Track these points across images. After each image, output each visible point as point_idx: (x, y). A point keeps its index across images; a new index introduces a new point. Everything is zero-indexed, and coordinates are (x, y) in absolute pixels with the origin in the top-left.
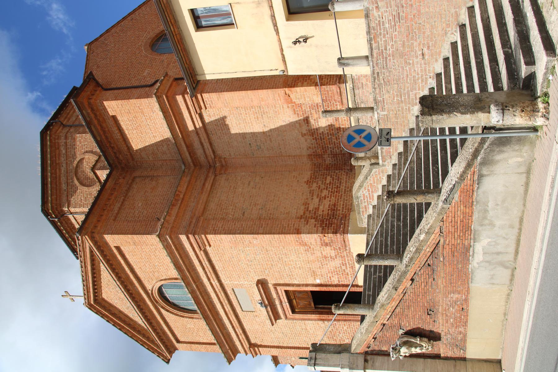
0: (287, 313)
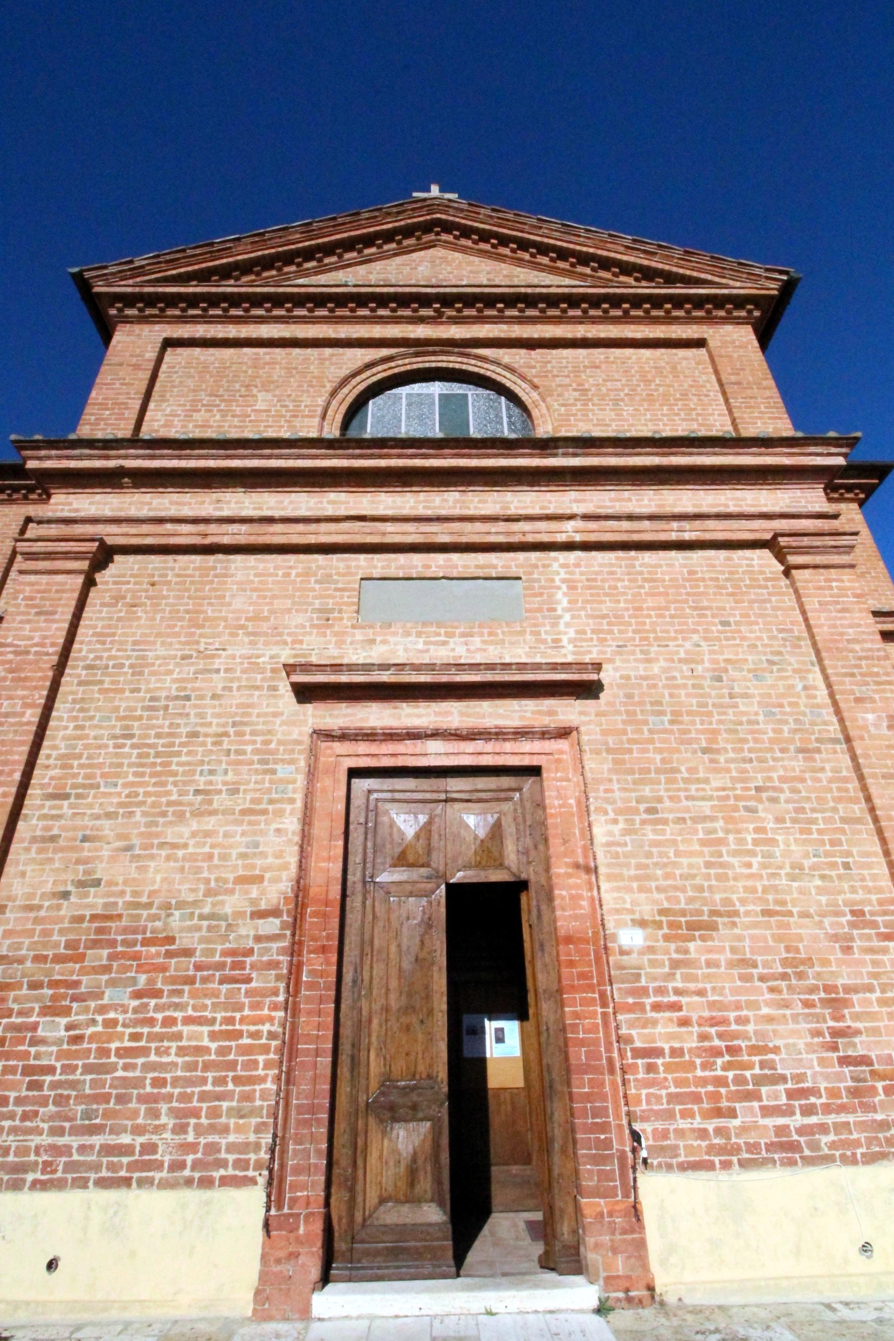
0: (363, 747)
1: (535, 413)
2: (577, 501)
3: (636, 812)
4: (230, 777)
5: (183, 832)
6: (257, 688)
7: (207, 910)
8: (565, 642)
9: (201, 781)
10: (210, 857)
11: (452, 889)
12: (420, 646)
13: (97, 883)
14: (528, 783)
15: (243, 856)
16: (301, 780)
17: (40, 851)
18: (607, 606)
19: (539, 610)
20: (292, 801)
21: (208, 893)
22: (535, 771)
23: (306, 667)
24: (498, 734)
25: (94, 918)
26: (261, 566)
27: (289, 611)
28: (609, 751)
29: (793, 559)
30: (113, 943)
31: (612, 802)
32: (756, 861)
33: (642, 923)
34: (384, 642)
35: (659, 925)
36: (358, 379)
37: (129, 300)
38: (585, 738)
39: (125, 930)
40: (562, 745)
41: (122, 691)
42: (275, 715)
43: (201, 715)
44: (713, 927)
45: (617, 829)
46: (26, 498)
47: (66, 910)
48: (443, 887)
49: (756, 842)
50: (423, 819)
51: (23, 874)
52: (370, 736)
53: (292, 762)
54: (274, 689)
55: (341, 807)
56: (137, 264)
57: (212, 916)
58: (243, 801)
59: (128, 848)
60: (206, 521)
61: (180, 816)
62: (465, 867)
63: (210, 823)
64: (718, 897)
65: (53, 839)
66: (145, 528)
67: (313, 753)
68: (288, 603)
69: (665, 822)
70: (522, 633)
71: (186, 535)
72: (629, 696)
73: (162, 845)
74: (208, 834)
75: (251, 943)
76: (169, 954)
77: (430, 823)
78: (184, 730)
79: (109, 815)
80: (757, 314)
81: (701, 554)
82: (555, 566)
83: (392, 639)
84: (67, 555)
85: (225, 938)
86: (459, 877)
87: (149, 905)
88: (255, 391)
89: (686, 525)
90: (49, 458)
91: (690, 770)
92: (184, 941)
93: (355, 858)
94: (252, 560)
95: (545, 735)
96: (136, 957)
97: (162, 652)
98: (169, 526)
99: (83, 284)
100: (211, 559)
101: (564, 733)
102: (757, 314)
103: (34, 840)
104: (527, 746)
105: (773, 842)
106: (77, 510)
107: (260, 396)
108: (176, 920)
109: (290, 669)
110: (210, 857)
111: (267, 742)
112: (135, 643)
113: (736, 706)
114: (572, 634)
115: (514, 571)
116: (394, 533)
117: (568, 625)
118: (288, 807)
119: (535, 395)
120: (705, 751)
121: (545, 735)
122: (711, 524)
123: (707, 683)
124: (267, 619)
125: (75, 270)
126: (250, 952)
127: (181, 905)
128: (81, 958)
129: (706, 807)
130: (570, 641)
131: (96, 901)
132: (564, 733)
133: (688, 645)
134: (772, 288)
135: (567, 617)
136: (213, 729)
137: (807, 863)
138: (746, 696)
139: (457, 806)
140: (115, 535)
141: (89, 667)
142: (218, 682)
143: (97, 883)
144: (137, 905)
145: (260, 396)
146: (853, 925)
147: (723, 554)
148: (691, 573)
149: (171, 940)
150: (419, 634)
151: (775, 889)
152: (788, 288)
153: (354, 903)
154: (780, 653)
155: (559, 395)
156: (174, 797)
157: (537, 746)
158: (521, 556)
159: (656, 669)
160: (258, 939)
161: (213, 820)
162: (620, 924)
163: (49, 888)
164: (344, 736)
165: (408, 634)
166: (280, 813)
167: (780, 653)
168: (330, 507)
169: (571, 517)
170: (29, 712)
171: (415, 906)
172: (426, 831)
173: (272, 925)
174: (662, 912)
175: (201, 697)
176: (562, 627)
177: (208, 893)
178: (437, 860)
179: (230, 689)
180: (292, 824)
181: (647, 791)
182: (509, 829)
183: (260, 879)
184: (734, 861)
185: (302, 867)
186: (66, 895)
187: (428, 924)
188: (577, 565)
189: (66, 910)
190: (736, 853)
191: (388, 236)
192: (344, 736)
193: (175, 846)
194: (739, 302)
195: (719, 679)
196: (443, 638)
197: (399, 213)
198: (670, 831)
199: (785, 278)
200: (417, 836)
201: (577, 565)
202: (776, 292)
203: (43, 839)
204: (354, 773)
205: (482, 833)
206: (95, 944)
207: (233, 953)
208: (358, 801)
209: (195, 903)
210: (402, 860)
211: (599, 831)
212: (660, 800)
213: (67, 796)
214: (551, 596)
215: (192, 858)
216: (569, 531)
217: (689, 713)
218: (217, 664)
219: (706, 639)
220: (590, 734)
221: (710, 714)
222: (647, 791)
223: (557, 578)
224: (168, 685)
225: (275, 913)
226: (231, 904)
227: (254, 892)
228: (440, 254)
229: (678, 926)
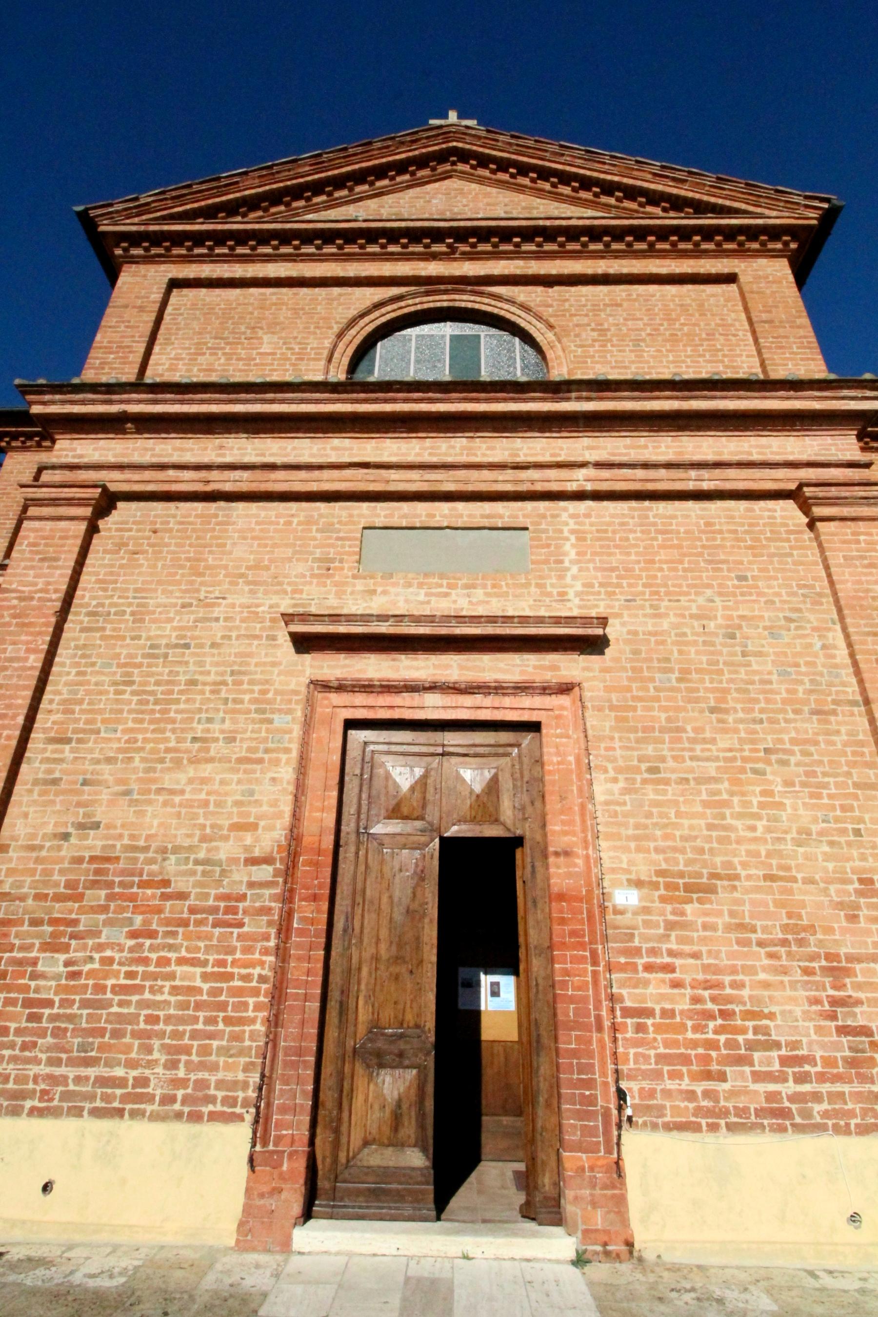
0: (360, 699)
1: (550, 354)
2: (589, 448)
3: (637, 770)
4: (227, 725)
5: (180, 778)
6: (256, 637)
7: (202, 855)
8: (571, 595)
9: (199, 729)
10: (206, 803)
11: (443, 840)
12: (422, 598)
13: (96, 826)
14: (527, 739)
15: (237, 803)
16: (297, 731)
17: (42, 793)
18: (616, 559)
19: (546, 562)
20: (287, 751)
21: (204, 839)
22: (534, 727)
23: (304, 617)
24: (497, 689)
25: (93, 859)
26: (263, 514)
27: (290, 560)
28: (612, 708)
29: (818, 511)
30: (110, 885)
31: (613, 760)
32: (760, 825)
33: (638, 884)
34: (385, 593)
35: (655, 886)
36: (367, 319)
37: (135, 239)
38: (587, 694)
39: (123, 873)
40: (564, 700)
41: (123, 638)
42: (274, 664)
43: (201, 664)
44: (712, 890)
45: (617, 787)
46: (39, 445)
47: (67, 851)
48: (437, 840)
49: (762, 806)
50: (418, 772)
51: (26, 815)
52: (367, 688)
53: (289, 712)
54: (274, 638)
55: (336, 758)
56: (142, 201)
57: (206, 862)
58: (240, 750)
59: (127, 793)
60: (208, 467)
61: (178, 762)
62: (459, 821)
63: (207, 770)
64: (718, 860)
65: (55, 782)
66: (148, 475)
67: (310, 703)
68: (289, 552)
69: (667, 782)
70: (527, 585)
71: (188, 481)
72: (636, 652)
73: (159, 791)
74: (204, 781)
75: (243, 889)
76: (165, 897)
77: (425, 776)
78: (183, 678)
79: (109, 760)
80: (793, 246)
81: (719, 504)
82: (564, 516)
83: (392, 590)
84: (70, 502)
85: (219, 883)
86: (453, 831)
87: (146, 849)
88: (260, 333)
89: (705, 473)
90: (53, 402)
91: (696, 730)
92: (179, 884)
93: (350, 809)
94: (254, 508)
95: (546, 690)
96: (133, 898)
97: (162, 599)
98: (171, 473)
99: (87, 222)
100: (213, 506)
101: (565, 689)
102: (793, 246)
103: (36, 782)
104: (526, 701)
105: (780, 806)
106: (81, 456)
107: (266, 338)
108: (172, 865)
109: (288, 618)
110: (206, 803)
111: (264, 692)
112: (136, 590)
113: (749, 664)
114: (579, 587)
115: (521, 522)
116: (397, 481)
117: (574, 578)
118: (284, 757)
119: (550, 335)
120: (712, 710)
121: (546, 690)
122: (732, 473)
123: (719, 640)
124: (268, 568)
125: (80, 208)
126: (243, 897)
127: (176, 850)
128: (80, 897)
129: (711, 768)
130: (577, 594)
131: (95, 843)
132: (565, 689)
133: (701, 600)
134: (811, 218)
135: (574, 570)
136: (212, 678)
137: (814, 828)
138: (760, 654)
139: (454, 760)
140: (117, 481)
141: (90, 614)
142: (217, 630)
143: (96, 826)
144: (135, 848)
145: (266, 338)
146: (860, 893)
147: (742, 505)
148: (708, 524)
149: (166, 883)
150: (420, 585)
151: (779, 854)
152: (829, 217)
153: (347, 854)
154: (799, 610)
155: (577, 336)
156: (172, 744)
157: (538, 701)
158: (529, 505)
159: (665, 625)
160: (251, 885)
161: (209, 767)
162: (616, 884)
163: (49, 829)
164: (341, 688)
165: (409, 585)
166: (276, 762)
167: (799, 610)
168: (333, 453)
169: (583, 465)
170: (32, 657)
171: (408, 858)
172: (422, 783)
173: (265, 872)
174: (660, 873)
175: (201, 646)
176: (568, 580)
177: (204, 839)
178: (432, 814)
179: (229, 638)
180: (287, 773)
181: (650, 750)
182: (506, 784)
183: (254, 827)
184: (738, 824)
185: (296, 816)
186: (66, 836)
187: (421, 876)
188: (588, 516)
189: (67, 851)
190: (740, 816)
191: (401, 167)
192: (341, 688)
193: (172, 792)
194: (774, 232)
195: (733, 636)
196: (444, 590)
197: (413, 142)
198: (671, 791)
199: (825, 206)
200: (412, 789)
201: (588, 516)
202: (815, 222)
203: (46, 782)
204: (351, 724)
205: (478, 788)
206: (94, 884)
207: (226, 897)
208: (353, 752)
209: (191, 849)
210: (396, 812)
211: (600, 790)
212: (663, 759)
213: (68, 741)
214: (558, 547)
215: (189, 804)
216: (579, 479)
217: (699, 671)
218: (216, 612)
219: (720, 594)
220: (593, 690)
221: (720, 672)
222: (650, 750)
223: (566, 529)
224: (168, 633)
225: (267, 860)
226: (225, 850)
227: (249, 839)
228: (455, 186)
229: (676, 887)
